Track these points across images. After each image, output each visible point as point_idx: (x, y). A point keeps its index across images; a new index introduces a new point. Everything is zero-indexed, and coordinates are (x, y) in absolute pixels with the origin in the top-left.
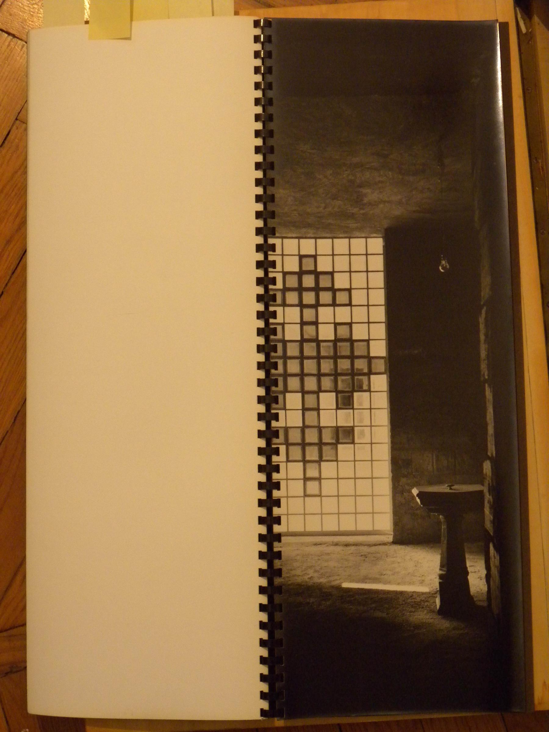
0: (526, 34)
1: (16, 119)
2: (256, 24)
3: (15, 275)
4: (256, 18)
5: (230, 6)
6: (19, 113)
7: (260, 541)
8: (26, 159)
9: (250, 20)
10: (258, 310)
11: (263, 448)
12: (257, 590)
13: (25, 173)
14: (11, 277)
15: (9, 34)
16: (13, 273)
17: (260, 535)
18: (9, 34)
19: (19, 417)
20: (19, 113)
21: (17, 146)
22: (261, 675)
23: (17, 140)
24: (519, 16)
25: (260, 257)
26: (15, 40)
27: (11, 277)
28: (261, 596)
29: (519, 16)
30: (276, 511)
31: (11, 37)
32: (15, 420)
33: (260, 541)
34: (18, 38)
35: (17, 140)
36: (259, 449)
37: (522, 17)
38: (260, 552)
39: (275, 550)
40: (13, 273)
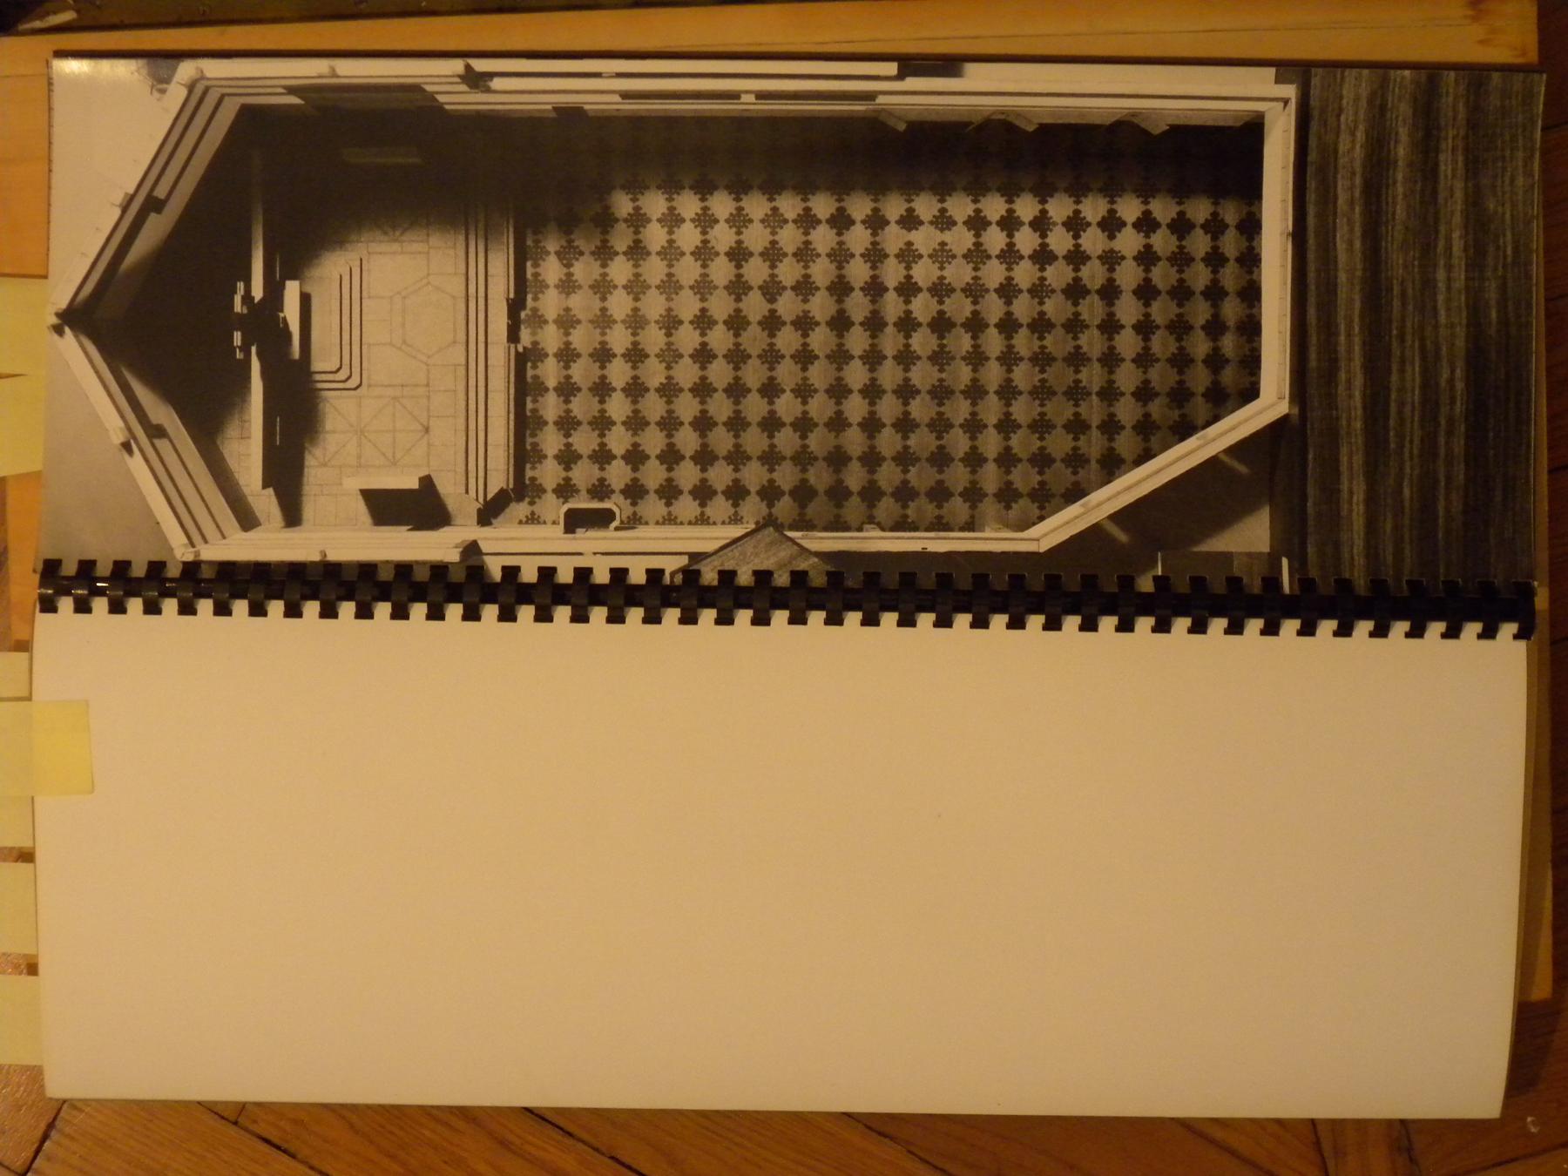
0: (78, 11)
1: (236, 1123)
2: (48, 606)
7: (1204, 632)
9: (43, 619)
13: (354, 1108)
14: (580, 1140)
15: (45, 1137)
16: (570, 1134)
18: (45, 1137)
21: (295, 1122)
23: (282, 1123)
24: (38, 24)
27: (580, 1140)
29: (38, 24)
31: (53, 1134)
34: (55, 1119)
36: (828, 622)
37: (42, 17)
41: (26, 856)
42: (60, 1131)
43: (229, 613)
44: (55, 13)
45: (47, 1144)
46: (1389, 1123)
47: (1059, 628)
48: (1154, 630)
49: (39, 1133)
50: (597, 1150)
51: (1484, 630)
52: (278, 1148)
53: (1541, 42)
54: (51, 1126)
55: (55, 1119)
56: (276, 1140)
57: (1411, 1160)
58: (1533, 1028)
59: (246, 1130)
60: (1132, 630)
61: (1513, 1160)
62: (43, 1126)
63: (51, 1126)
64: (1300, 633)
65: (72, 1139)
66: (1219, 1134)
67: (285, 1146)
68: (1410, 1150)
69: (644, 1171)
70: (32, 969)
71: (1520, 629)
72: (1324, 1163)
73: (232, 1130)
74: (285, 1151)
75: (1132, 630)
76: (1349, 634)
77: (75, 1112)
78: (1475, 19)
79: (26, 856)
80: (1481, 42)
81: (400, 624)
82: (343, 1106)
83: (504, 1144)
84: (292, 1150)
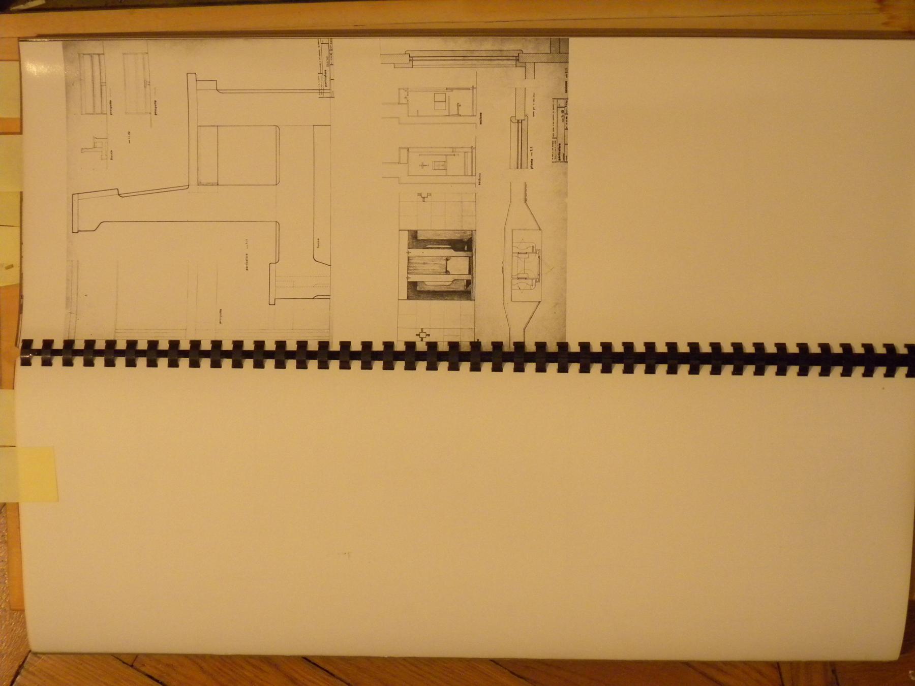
1: (132, 666)
2: (26, 363)
3: (336, 672)
4: (19, 361)
5: (5, 393)
7: (676, 373)
8: (186, 656)
9: (21, 370)
10: (490, 370)
11: (493, 365)
13: (203, 657)
14: (338, 678)
15: (17, 673)
16: (332, 675)
17: (778, 374)
18: (17, 673)
19: (132, 662)
21: (168, 665)
22: (843, 375)
23: (160, 666)
24: (22, 7)
26: (26, 666)
27: (338, 678)
28: (592, 371)
29: (22, 7)
30: (508, 347)
31: (23, 672)
32: (521, 678)
33: (676, 373)
34: (24, 662)
35: (160, 666)
36: (450, 369)
38: (690, 373)
39: (512, 349)
40: (332, 675)
41: (328, 297)
43: (135, 366)
46: (825, 664)
47: (588, 372)
55: (24, 662)
56: (156, 677)
59: (139, 671)
60: (654, 373)
62: (16, 668)
64: (865, 375)
65: (34, 674)
73: (130, 671)
75: (654, 373)
78: (881, 10)
79: (328, 297)
81: (174, 338)
82: (197, 656)
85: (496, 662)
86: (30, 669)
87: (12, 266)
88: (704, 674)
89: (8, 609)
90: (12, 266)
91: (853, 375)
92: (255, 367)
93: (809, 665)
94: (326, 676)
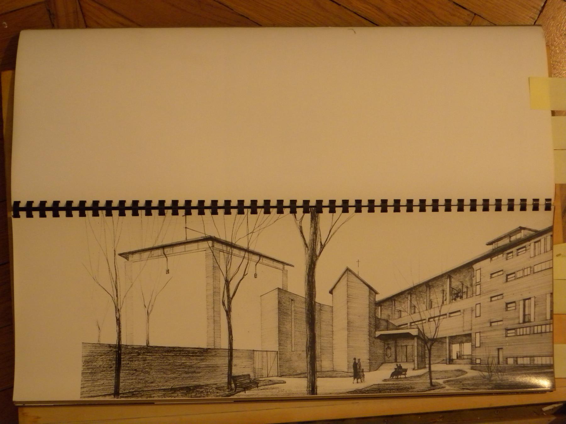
0: (542, 411)
1: (475, 14)
4: (552, 202)
6: (480, 16)
12: (149, 199)
15: (543, 7)
16: (355, 13)
17: (124, 202)
19: (474, 18)
20: (480, 16)
21: (454, 15)
23: (459, 14)
24: (556, 405)
25: (102, 204)
26: (538, 12)
29: (556, 405)
31: (540, 8)
32: (242, 15)
34: (540, 14)
37: (555, 408)
40: (355, 13)
42: (537, 9)
44: (550, 410)
45: (542, 5)
48: (59, 202)
49: (545, 9)
50: (346, 8)
51: (32, 204)
52: (460, 6)
53: (17, 419)
54: (541, 12)
55: (540, 14)
57: (49, 11)
58: (10, 63)
61: (11, 12)
62: (544, 11)
63: (541, 12)
65: (534, 7)
66: (121, 19)
67: (457, 7)
68: (50, 14)
69: (331, 2)
70: (553, 113)
71: (58, 205)
72: (81, 10)
73: (476, 11)
74: (457, 4)
76: (41, 202)
77: (533, 16)
80: (38, 418)
83: (379, 9)
84: (455, 5)
85: (257, 24)
86: (535, 10)
87: (557, 256)
88: (132, 21)
89: (550, 46)
90: (557, 256)
91: (39, 202)
92: (348, 201)
93: (69, 26)
94: (359, 12)
